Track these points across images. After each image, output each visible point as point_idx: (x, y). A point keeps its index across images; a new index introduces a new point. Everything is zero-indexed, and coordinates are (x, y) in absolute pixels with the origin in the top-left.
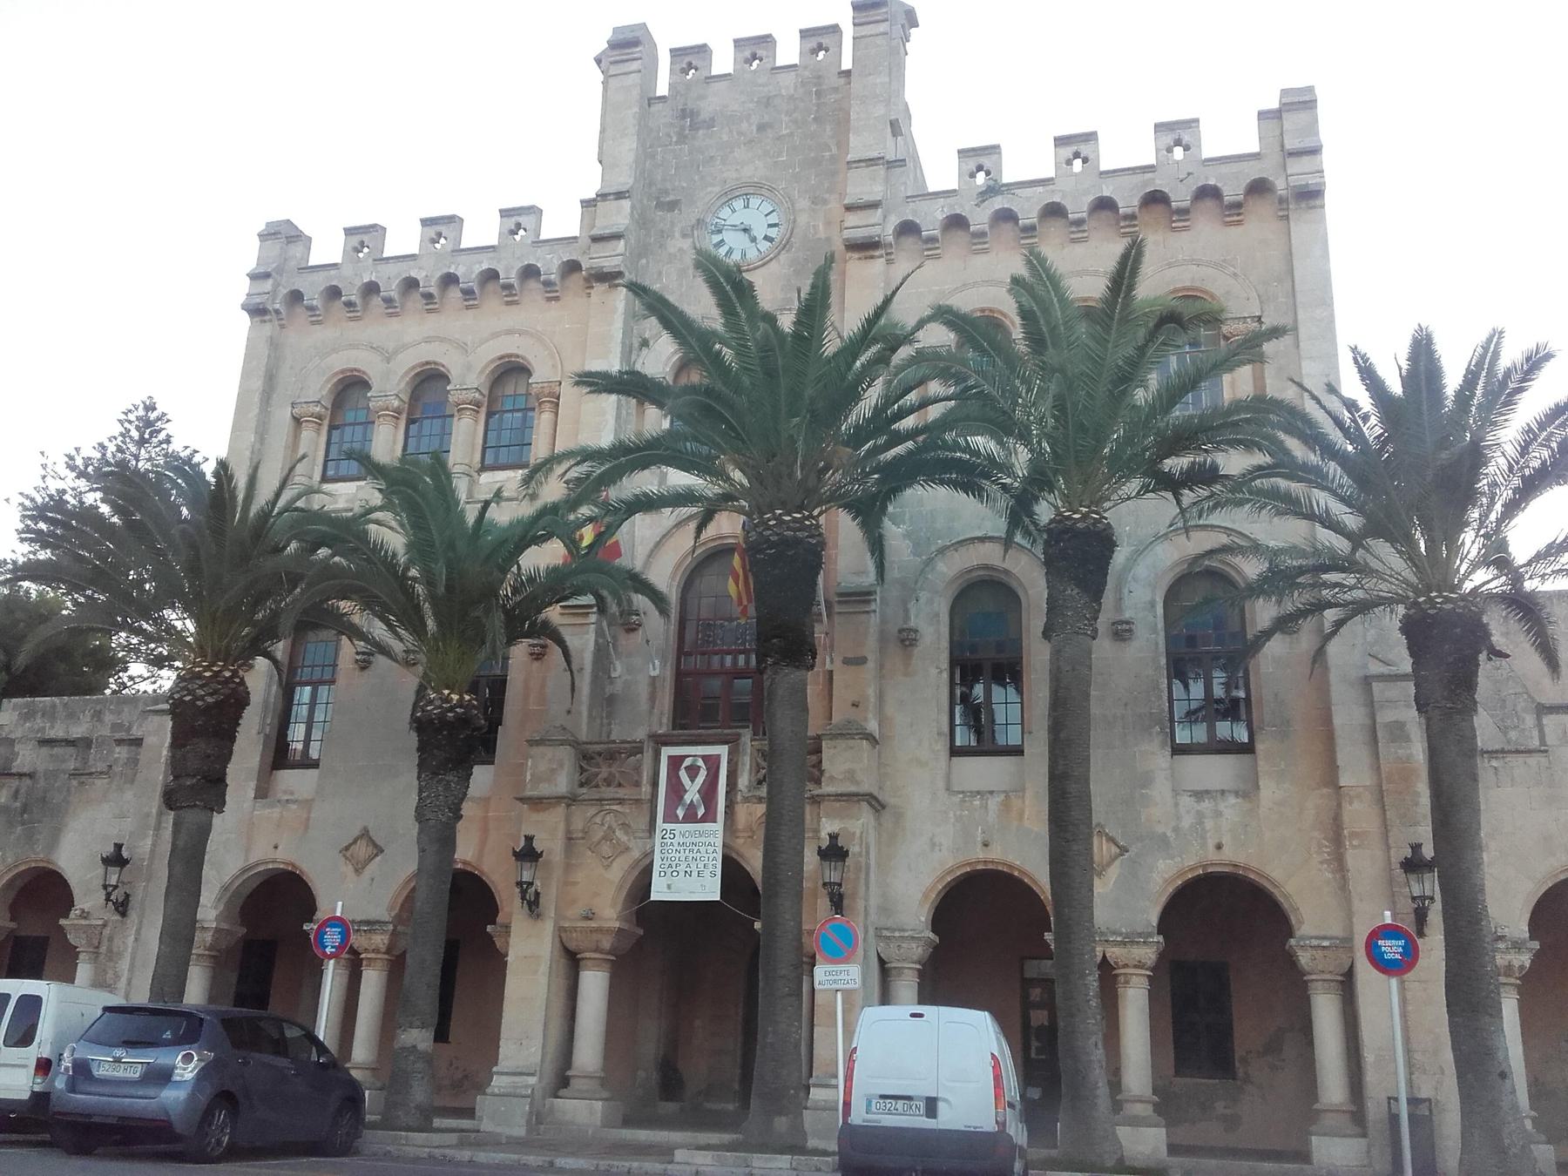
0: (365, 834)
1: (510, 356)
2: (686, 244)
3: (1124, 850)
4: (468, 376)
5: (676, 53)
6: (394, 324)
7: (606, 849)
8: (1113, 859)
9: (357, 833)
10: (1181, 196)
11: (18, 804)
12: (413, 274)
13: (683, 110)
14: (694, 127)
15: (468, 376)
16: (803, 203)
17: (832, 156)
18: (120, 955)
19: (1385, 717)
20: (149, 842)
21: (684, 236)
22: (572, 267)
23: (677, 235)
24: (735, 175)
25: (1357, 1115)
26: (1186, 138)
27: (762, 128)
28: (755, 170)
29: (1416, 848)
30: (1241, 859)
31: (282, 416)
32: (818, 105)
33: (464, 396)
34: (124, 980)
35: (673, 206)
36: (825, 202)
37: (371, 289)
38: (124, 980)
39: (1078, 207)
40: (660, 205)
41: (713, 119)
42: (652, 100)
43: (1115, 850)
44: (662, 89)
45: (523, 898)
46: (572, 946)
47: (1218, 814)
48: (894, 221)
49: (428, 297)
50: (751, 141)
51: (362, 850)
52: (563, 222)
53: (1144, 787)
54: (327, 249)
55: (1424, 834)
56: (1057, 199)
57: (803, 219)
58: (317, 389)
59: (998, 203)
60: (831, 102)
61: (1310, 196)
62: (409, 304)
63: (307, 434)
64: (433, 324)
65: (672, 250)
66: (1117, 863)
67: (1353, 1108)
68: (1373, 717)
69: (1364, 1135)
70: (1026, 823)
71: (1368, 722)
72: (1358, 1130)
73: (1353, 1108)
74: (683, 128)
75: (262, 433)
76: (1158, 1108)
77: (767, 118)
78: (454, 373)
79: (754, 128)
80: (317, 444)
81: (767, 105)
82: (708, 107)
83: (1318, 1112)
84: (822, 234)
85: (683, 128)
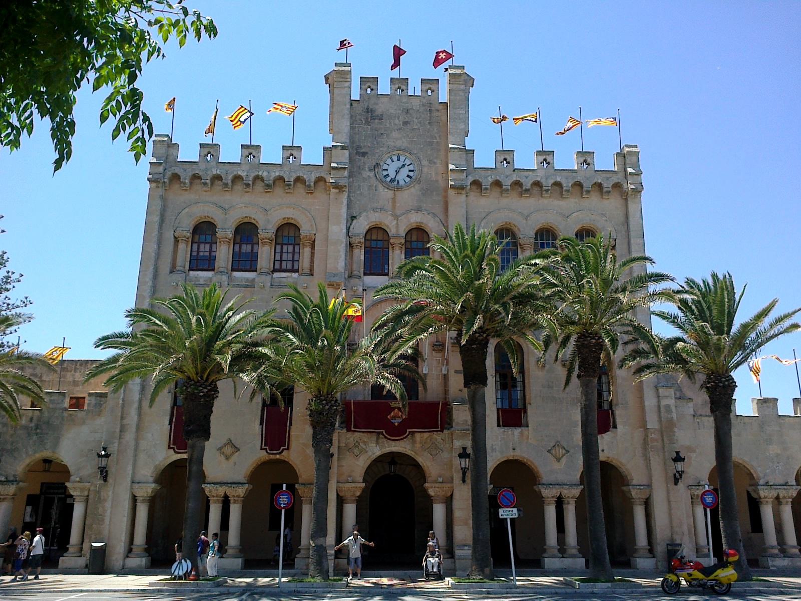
0: (230, 443)
1: (288, 218)
2: (372, 174)
3: (568, 451)
4: (267, 225)
5: (363, 80)
6: (228, 196)
7: (356, 451)
8: (563, 455)
9: (225, 441)
10: (587, 185)
11: (33, 425)
12: (240, 173)
13: (368, 109)
14: (373, 118)
15: (267, 225)
16: (425, 162)
17: (438, 142)
18: (105, 500)
19: (664, 402)
20: (116, 445)
21: (370, 170)
22: (320, 180)
23: (367, 169)
24: (393, 144)
25: (651, 551)
26: (589, 160)
27: (406, 123)
28: (403, 143)
29: (464, 449)
30: (525, 455)
31: (169, 236)
32: (430, 117)
33: (266, 235)
34: (109, 512)
35: (364, 154)
36: (435, 163)
37: (218, 178)
38: (109, 512)
39: (548, 183)
40: (357, 153)
41: (382, 115)
42: (352, 102)
43: (564, 451)
44: (355, 96)
45: (101, 474)
46: (341, 494)
47: (513, 434)
48: (471, 179)
49: (248, 185)
50: (400, 129)
51: (228, 450)
52: (312, 156)
53: (575, 427)
54: (188, 153)
55: (468, 443)
56: (539, 179)
57: (425, 170)
58: (187, 224)
59: (515, 178)
60: (435, 117)
61: (638, 191)
62: (236, 187)
63: (182, 246)
64: (247, 198)
65: (364, 176)
66: (565, 457)
67: (649, 547)
68: (659, 401)
69: (654, 557)
70: (530, 441)
71: (657, 404)
72: (651, 556)
73: (649, 547)
74: (367, 118)
75: (159, 243)
76: (579, 551)
77: (407, 119)
78: (261, 225)
79: (401, 123)
80: (186, 252)
81: (407, 112)
82: (380, 109)
83: (636, 549)
84: (434, 179)
85: (367, 118)
